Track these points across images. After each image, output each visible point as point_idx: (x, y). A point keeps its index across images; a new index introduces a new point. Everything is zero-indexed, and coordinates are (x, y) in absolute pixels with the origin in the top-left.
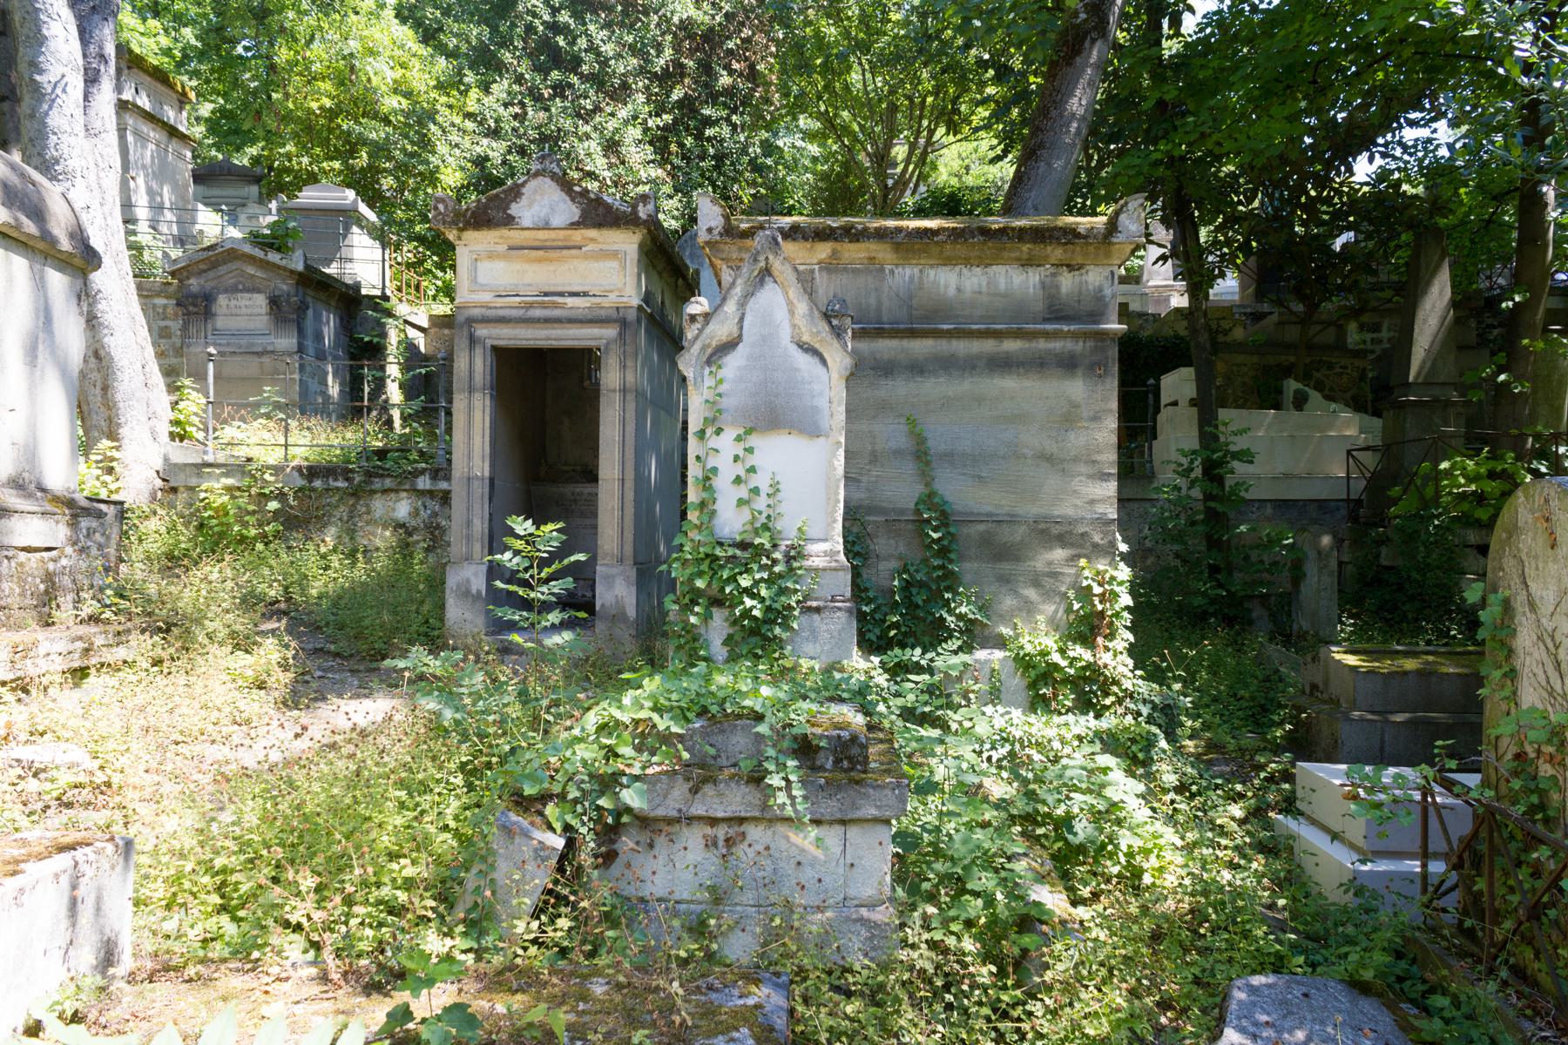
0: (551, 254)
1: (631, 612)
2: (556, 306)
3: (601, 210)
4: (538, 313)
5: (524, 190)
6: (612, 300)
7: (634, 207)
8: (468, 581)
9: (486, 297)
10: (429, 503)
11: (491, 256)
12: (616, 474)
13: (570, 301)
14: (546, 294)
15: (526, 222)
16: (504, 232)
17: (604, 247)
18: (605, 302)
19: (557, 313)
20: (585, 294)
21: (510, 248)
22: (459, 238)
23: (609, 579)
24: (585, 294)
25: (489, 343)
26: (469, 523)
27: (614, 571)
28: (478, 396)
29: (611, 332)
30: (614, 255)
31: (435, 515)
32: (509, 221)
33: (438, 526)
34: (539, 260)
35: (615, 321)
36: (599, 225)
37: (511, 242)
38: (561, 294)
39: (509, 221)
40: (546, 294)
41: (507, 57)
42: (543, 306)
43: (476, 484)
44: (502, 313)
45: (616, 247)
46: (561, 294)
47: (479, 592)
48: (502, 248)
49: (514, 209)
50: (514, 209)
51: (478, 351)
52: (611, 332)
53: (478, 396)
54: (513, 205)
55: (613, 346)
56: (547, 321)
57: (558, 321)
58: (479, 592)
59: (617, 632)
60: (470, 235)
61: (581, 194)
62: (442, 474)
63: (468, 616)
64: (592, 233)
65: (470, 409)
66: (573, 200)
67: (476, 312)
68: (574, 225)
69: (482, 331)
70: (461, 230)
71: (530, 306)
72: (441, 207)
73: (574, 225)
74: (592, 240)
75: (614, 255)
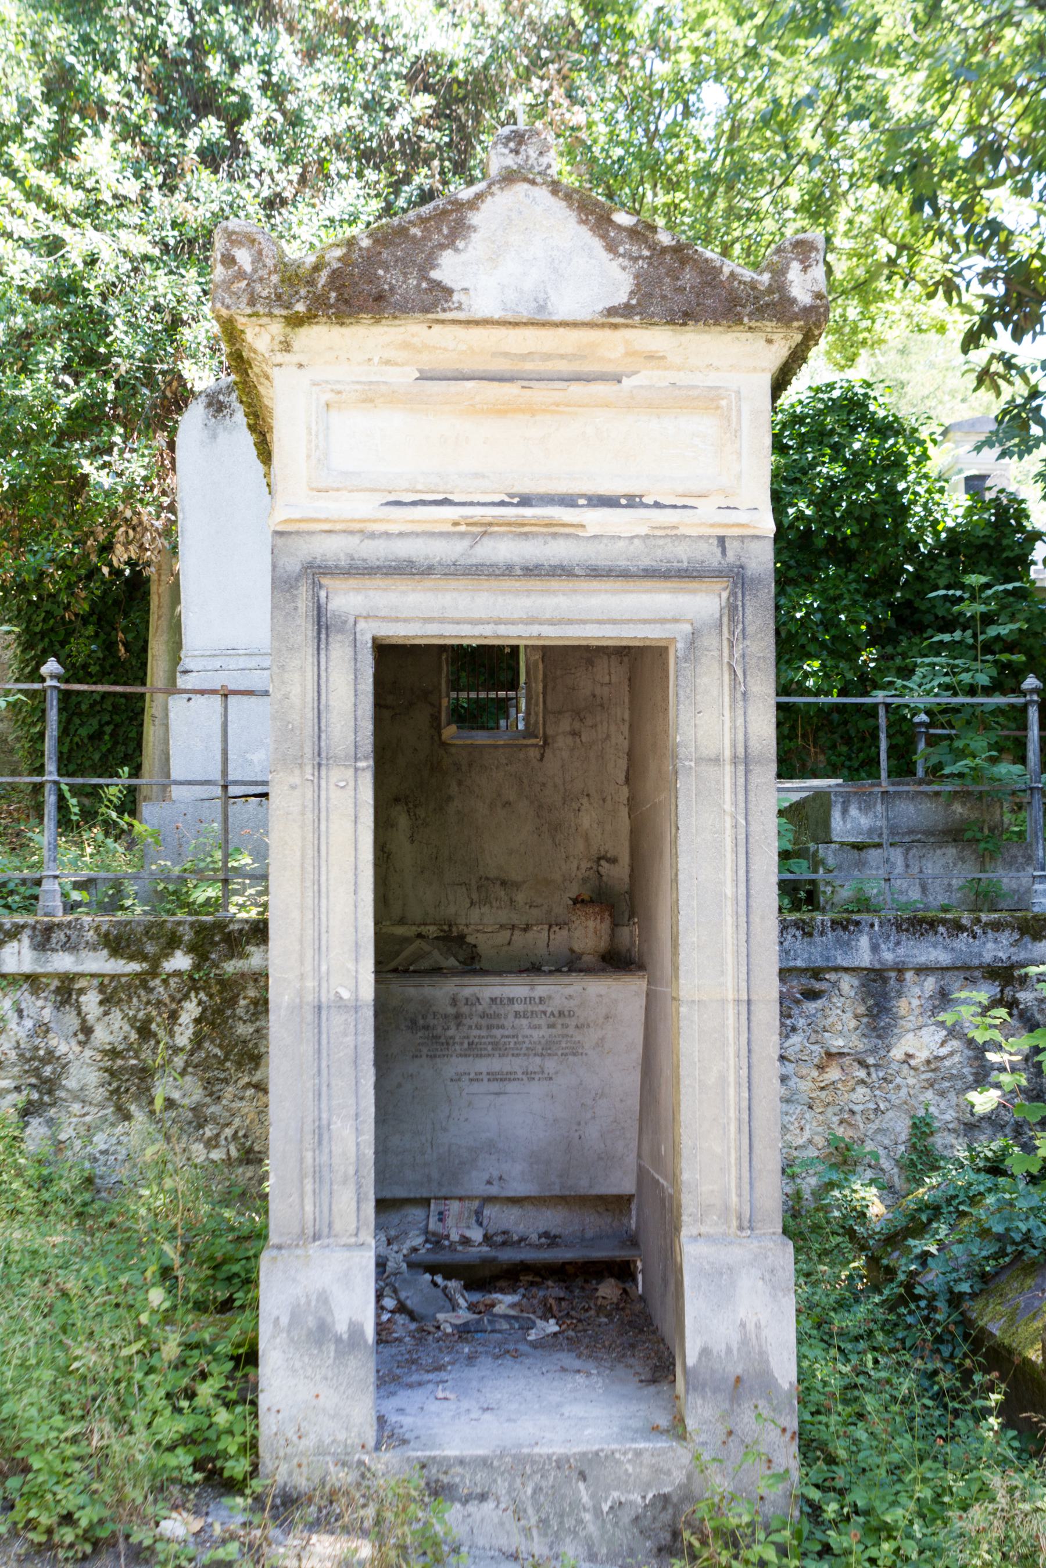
0: (541, 394)
1: (785, 1371)
2: (553, 530)
3: (688, 277)
4: (502, 550)
5: (474, 218)
6: (705, 519)
7: (779, 272)
8: (324, 1298)
9: (362, 507)
10: (32, 1004)
11: (371, 397)
12: (730, 987)
13: (595, 519)
14: (525, 501)
15: (483, 305)
16: (412, 331)
17: (683, 378)
18: (688, 523)
19: (557, 551)
20: (633, 502)
21: (424, 377)
22: (286, 346)
23: (723, 1277)
24: (633, 502)
25: (368, 630)
26: (321, 1133)
27: (737, 1253)
28: (338, 776)
29: (705, 603)
30: (710, 400)
31: (43, 1029)
32: (435, 299)
33: (50, 1056)
34: (502, 411)
35: (718, 574)
36: (684, 317)
37: (429, 361)
38: (568, 501)
39: (435, 299)
40: (525, 501)
41: (109, 87)
42: (520, 530)
43: (337, 1022)
44: (404, 549)
45: (712, 379)
46: (568, 501)
47: (355, 1330)
48: (404, 376)
49: (448, 268)
50: (448, 268)
51: (339, 652)
52: (705, 603)
53: (338, 776)
54: (447, 259)
55: (710, 641)
56: (532, 571)
57: (562, 572)
58: (355, 1330)
59: (746, 1420)
60: (319, 336)
61: (633, 233)
62: (58, 936)
63: (330, 1399)
64: (659, 339)
65: (318, 810)
66: (611, 248)
67: (332, 548)
68: (619, 315)
69: (345, 599)
70: (296, 321)
71: (485, 530)
72: (244, 257)
73: (619, 315)
74: (651, 357)
75: (710, 400)
